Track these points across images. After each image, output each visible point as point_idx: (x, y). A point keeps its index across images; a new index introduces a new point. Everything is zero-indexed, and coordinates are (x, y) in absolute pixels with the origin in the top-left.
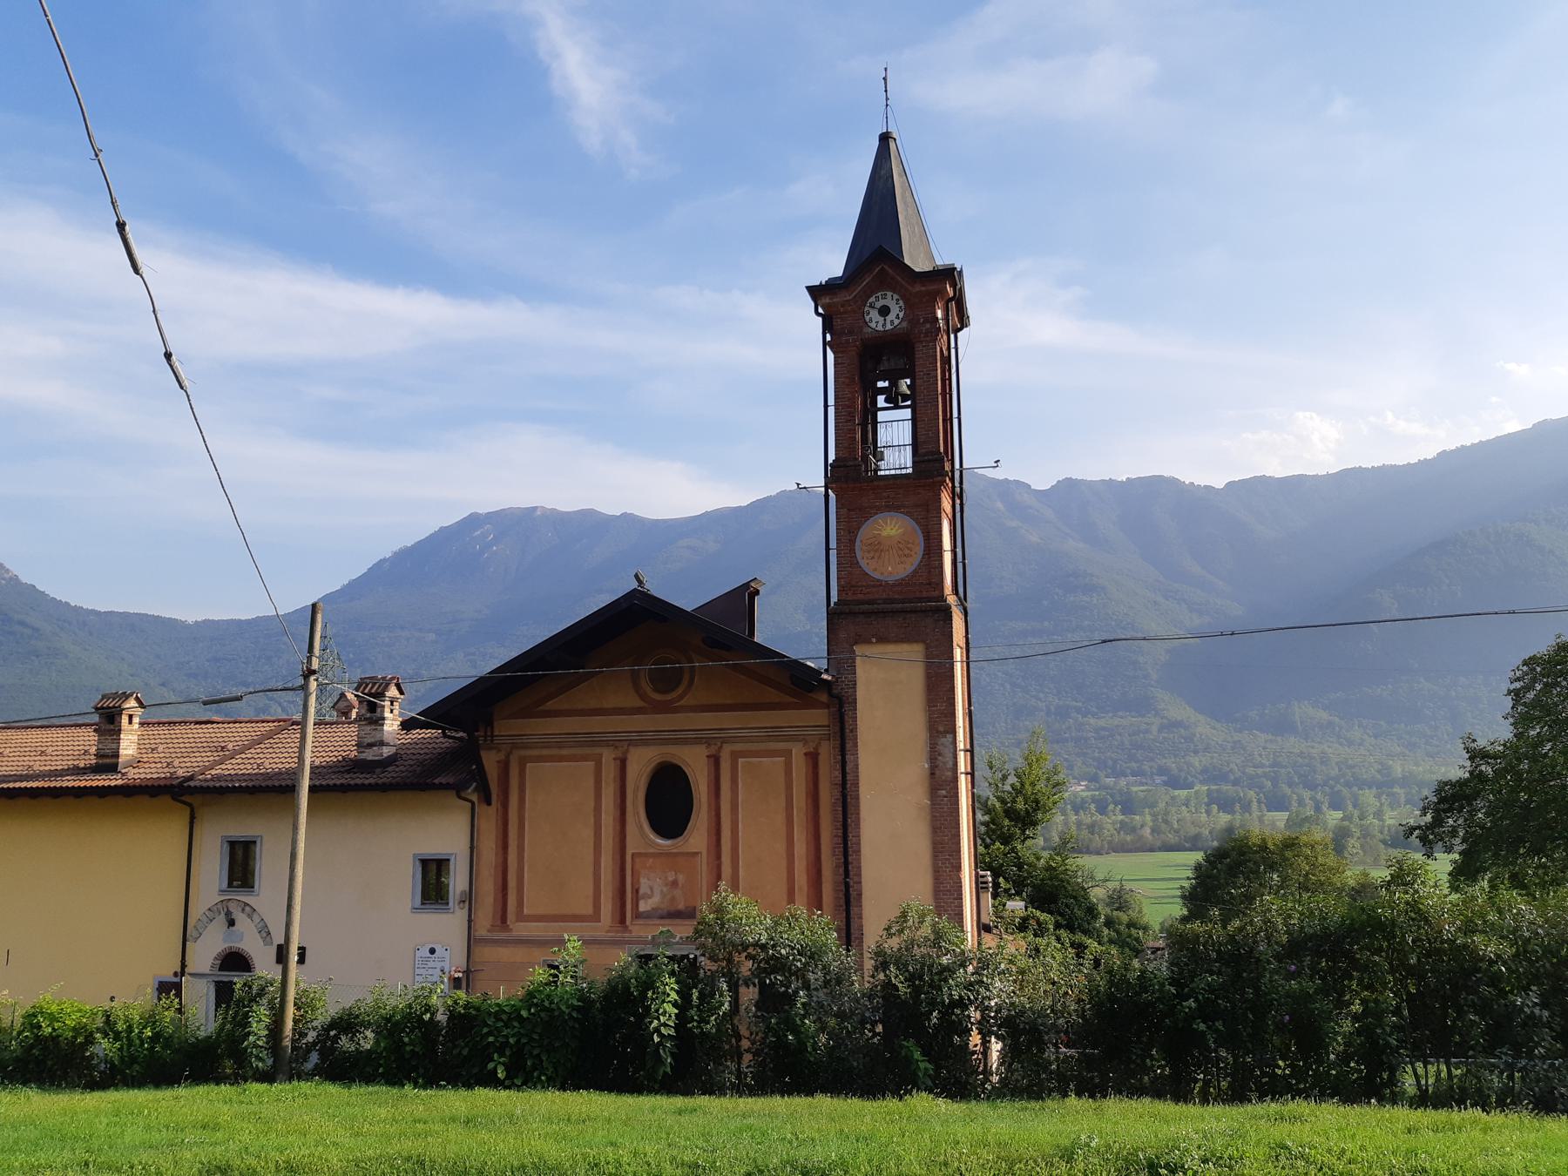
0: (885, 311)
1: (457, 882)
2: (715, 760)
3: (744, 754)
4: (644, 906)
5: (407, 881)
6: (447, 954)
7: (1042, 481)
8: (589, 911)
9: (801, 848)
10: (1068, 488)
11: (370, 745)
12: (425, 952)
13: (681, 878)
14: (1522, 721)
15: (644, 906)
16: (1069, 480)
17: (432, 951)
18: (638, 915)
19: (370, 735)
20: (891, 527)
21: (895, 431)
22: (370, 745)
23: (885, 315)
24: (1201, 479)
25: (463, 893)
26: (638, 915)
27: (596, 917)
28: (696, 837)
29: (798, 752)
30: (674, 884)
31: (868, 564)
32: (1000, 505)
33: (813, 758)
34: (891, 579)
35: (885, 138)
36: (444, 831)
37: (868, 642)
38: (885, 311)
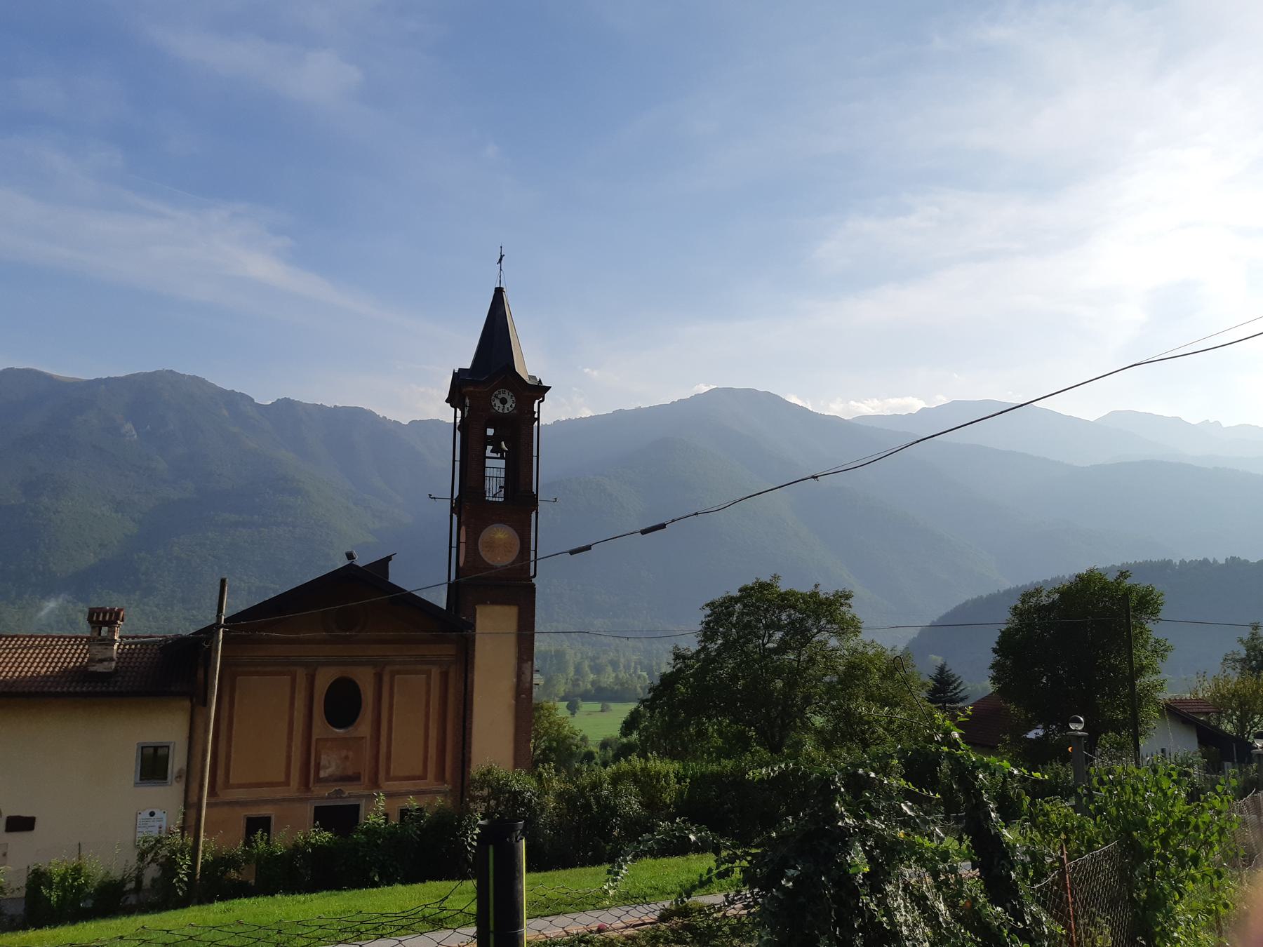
0: (504, 401)
1: (177, 762)
2: (379, 678)
3: (399, 672)
4: (322, 774)
5: (130, 764)
6: (164, 816)
7: (265, 398)
8: (282, 778)
9: (433, 733)
10: (286, 405)
11: (101, 661)
12: (146, 815)
13: (351, 754)
14: (708, 633)
15: (322, 774)
16: (287, 401)
17: (152, 814)
18: (319, 780)
19: (99, 652)
20: (500, 534)
21: (495, 467)
22: (101, 661)
23: (504, 404)
24: (392, 416)
25: (180, 770)
26: (319, 780)
27: (287, 783)
28: (363, 728)
29: (435, 671)
30: (347, 758)
31: (486, 556)
32: (225, 412)
33: (445, 676)
34: (499, 565)
35: (499, 292)
36: (167, 728)
37: (484, 603)
38: (504, 401)
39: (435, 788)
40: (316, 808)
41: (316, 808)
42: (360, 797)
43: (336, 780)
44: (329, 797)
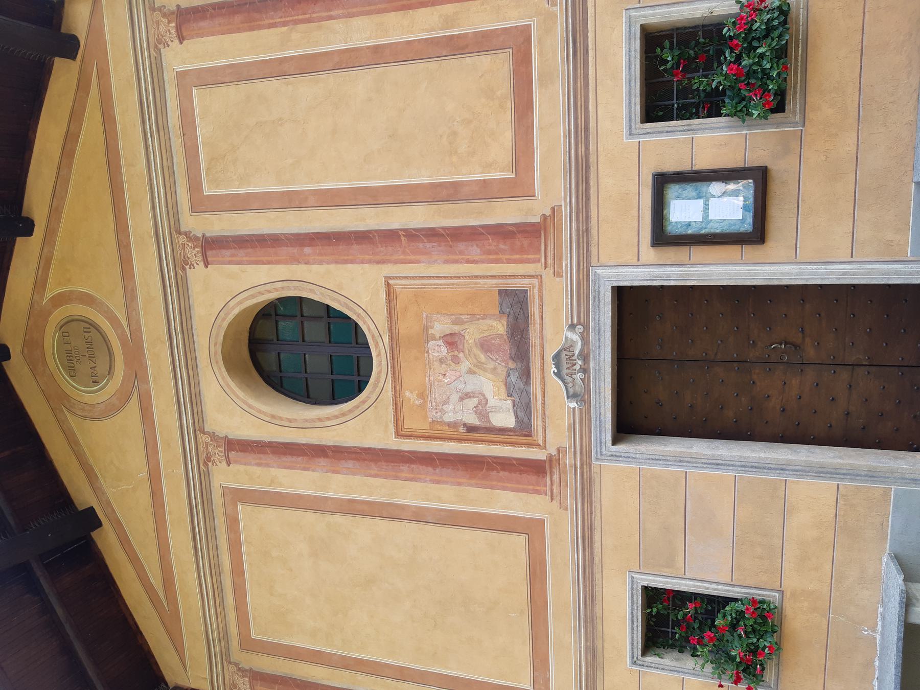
2: (211, 246)
3: (195, 186)
4: (505, 418)
13: (441, 327)
15: (505, 418)
18: (523, 430)
27: (531, 529)
28: (352, 288)
30: (452, 341)
39: (569, 261)
40: (542, 522)
41: (542, 522)
42: (583, 291)
43: (526, 374)
44: (580, 396)
